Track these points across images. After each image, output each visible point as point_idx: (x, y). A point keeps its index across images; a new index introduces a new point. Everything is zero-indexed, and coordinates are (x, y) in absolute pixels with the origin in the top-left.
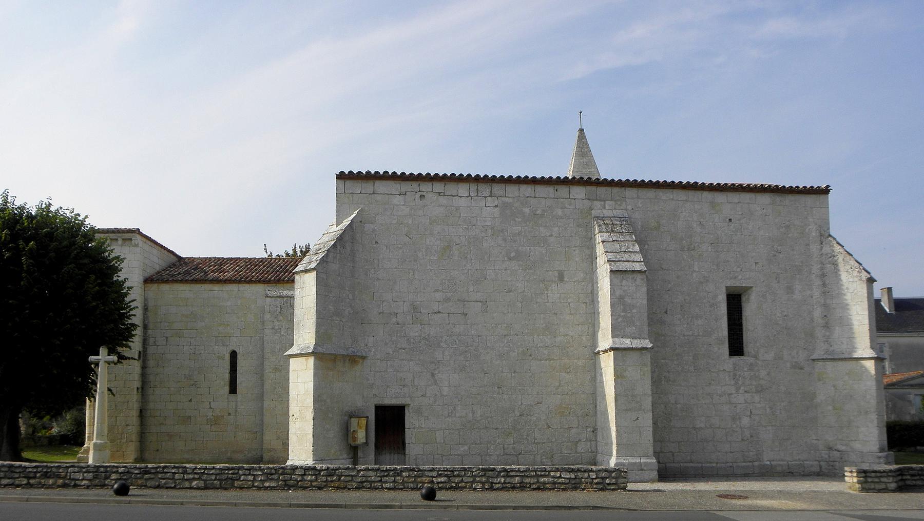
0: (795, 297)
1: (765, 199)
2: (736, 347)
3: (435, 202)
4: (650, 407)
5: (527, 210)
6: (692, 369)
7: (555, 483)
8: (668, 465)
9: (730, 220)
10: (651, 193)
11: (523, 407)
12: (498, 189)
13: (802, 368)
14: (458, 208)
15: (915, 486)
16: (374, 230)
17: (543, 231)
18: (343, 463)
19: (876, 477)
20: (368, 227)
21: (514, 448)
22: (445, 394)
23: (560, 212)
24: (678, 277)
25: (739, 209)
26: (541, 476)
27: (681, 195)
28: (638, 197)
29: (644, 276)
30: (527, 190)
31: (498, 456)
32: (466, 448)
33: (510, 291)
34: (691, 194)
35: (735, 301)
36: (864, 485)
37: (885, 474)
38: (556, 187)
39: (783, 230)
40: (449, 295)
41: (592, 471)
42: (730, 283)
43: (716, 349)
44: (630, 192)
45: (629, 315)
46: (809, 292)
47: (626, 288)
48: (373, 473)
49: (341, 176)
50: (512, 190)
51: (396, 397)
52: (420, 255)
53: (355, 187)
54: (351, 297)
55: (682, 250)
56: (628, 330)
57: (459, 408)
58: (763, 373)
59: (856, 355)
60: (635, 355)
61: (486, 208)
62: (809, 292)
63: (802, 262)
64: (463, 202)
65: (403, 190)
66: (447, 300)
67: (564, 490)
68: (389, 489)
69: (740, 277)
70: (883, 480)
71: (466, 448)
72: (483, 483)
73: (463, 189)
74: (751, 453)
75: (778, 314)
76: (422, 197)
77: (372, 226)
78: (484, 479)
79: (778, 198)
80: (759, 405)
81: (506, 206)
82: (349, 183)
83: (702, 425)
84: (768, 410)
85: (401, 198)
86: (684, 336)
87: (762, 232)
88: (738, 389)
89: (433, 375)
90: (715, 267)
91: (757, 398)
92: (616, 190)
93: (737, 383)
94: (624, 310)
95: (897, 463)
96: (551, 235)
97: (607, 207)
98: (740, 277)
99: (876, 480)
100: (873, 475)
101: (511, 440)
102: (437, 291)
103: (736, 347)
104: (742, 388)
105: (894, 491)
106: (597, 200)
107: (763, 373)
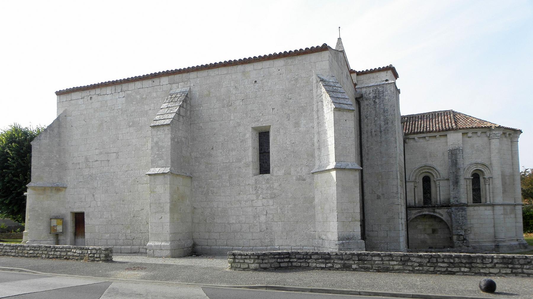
0: (300, 129)
1: (280, 62)
2: (264, 167)
3: (97, 99)
4: (168, 210)
5: (138, 96)
6: (228, 184)
7: (73, 256)
8: (212, 247)
9: (256, 82)
10: (205, 73)
11: (135, 212)
12: (125, 86)
13: (304, 180)
14: (106, 101)
15: (300, 266)
16: (71, 120)
17: (146, 108)
18: (49, 242)
19: (242, 259)
20: (69, 118)
21: (130, 235)
22: (99, 205)
23: (154, 95)
24: (221, 125)
25: (262, 73)
26: (69, 251)
27: (224, 70)
28: (197, 77)
29: (169, 127)
30: (138, 84)
31: (123, 240)
32: (109, 235)
33: (129, 145)
34: (230, 69)
35: (263, 137)
36: (234, 265)
37: (248, 257)
38: (153, 80)
39: (293, 82)
40: (102, 150)
41: (89, 249)
42: (254, 125)
43: (244, 171)
44: (193, 75)
45: (161, 153)
46: (311, 125)
47: (159, 136)
48: (8, 248)
49: (59, 93)
50: (131, 86)
51: (79, 208)
52: (89, 130)
53: (64, 98)
54: (57, 156)
55: (224, 107)
56: (160, 162)
57: (105, 213)
58: (276, 185)
59: (328, 168)
60: (161, 178)
61: (115, 99)
62: (311, 125)
63: (306, 103)
64: (108, 97)
65: (83, 96)
66: (101, 153)
67: (77, 260)
68: (13, 256)
69: (261, 120)
70: (246, 261)
71: (109, 235)
72: (46, 254)
73: (108, 90)
74: (266, 240)
75: (288, 143)
76: (91, 98)
77: (70, 118)
78: (46, 252)
79: (289, 60)
80: (272, 207)
81: (129, 96)
82: (62, 96)
83: (234, 221)
84: (279, 210)
85: (82, 100)
86: (224, 163)
87: (277, 87)
88: (258, 197)
89: (93, 195)
90: (245, 116)
91: (271, 202)
92: (185, 75)
93: (257, 193)
94: (158, 150)
95: (366, 250)
96: (150, 109)
97: (180, 87)
98: (261, 120)
99: (242, 261)
100: (239, 257)
101: (129, 231)
102: (96, 149)
103: (264, 167)
104: (261, 196)
105: (255, 270)
106: (174, 83)
107: (276, 185)
